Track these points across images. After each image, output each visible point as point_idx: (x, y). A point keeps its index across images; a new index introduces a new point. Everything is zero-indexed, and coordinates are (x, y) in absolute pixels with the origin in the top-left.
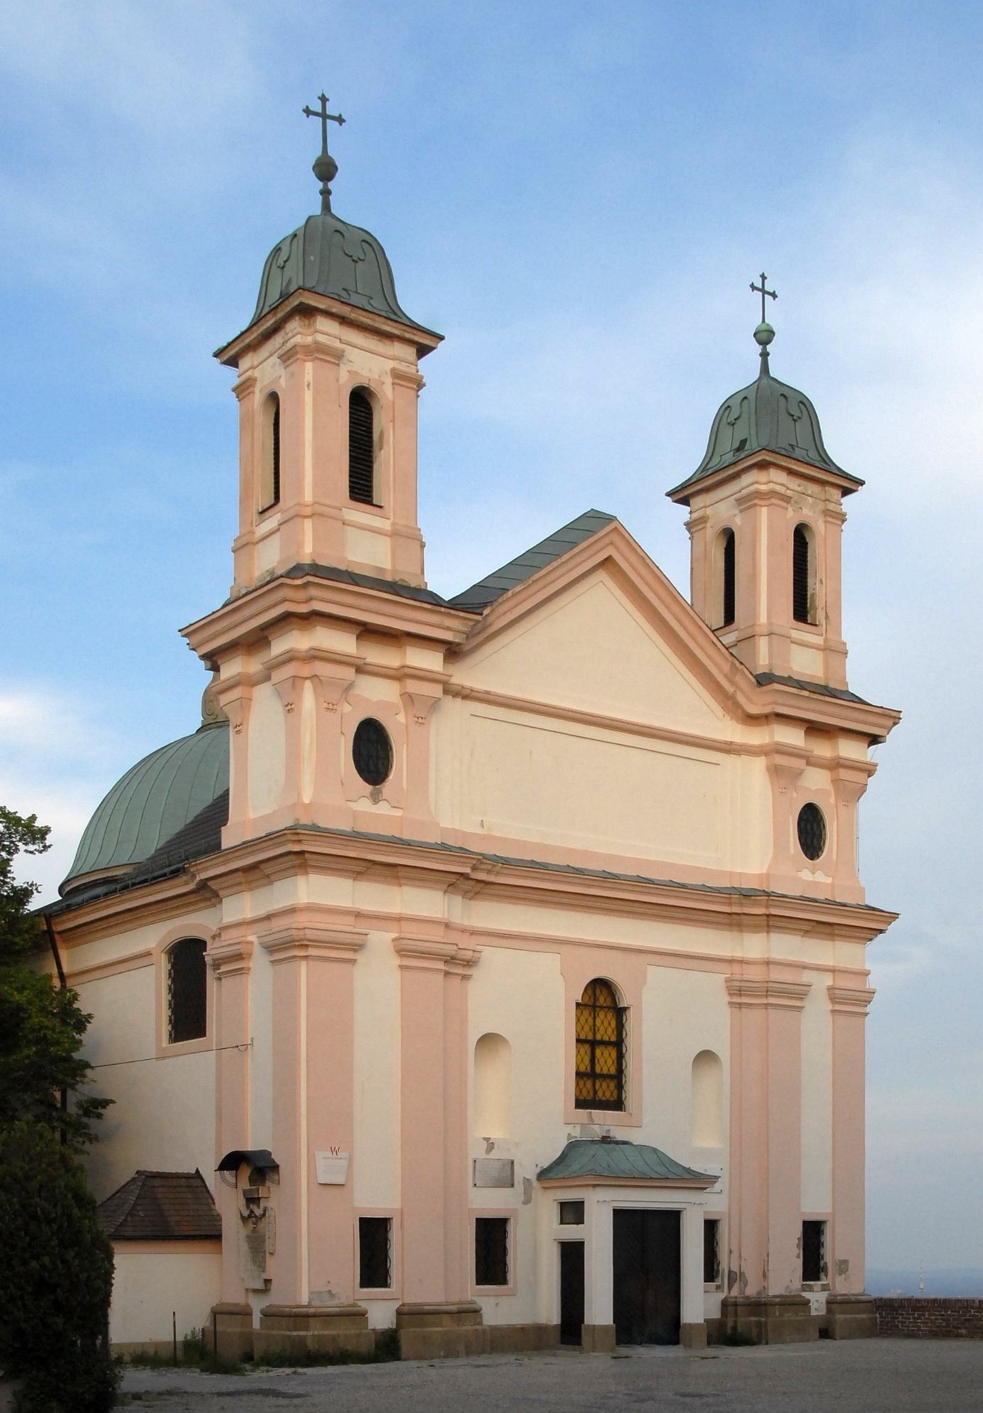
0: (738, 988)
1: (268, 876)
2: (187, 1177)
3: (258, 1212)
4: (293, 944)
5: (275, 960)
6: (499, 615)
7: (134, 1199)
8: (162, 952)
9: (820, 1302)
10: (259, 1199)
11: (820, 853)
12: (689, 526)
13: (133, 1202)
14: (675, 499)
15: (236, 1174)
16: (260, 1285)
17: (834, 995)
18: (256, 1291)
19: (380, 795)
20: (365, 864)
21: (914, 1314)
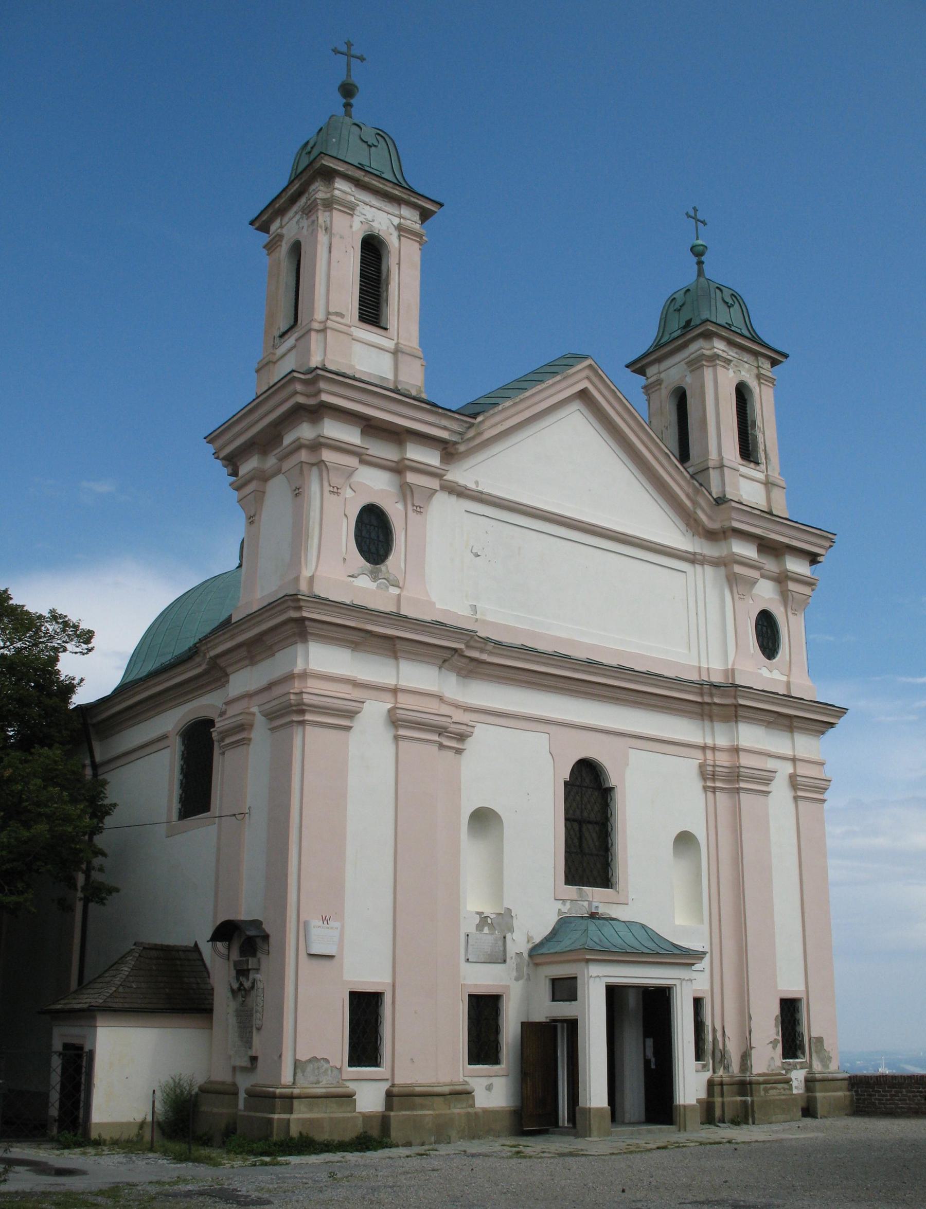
0: (711, 773)
1: (270, 647)
2: (186, 950)
3: (247, 985)
4: (290, 709)
5: (273, 728)
6: (490, 425)
7: (129, 970)
8: (177, 734)
9: (799, 1080)
10: (248, 970)
11: (775, 653)
12: (645, 388)
13: (127, 973)
14: (632, 370)
15: (229, 945)
16: (244, 1062)
17: (794, 782)
18: (244, 1069)
19: (380, 574)
20: (363, 635)
21: (891, 1091)
